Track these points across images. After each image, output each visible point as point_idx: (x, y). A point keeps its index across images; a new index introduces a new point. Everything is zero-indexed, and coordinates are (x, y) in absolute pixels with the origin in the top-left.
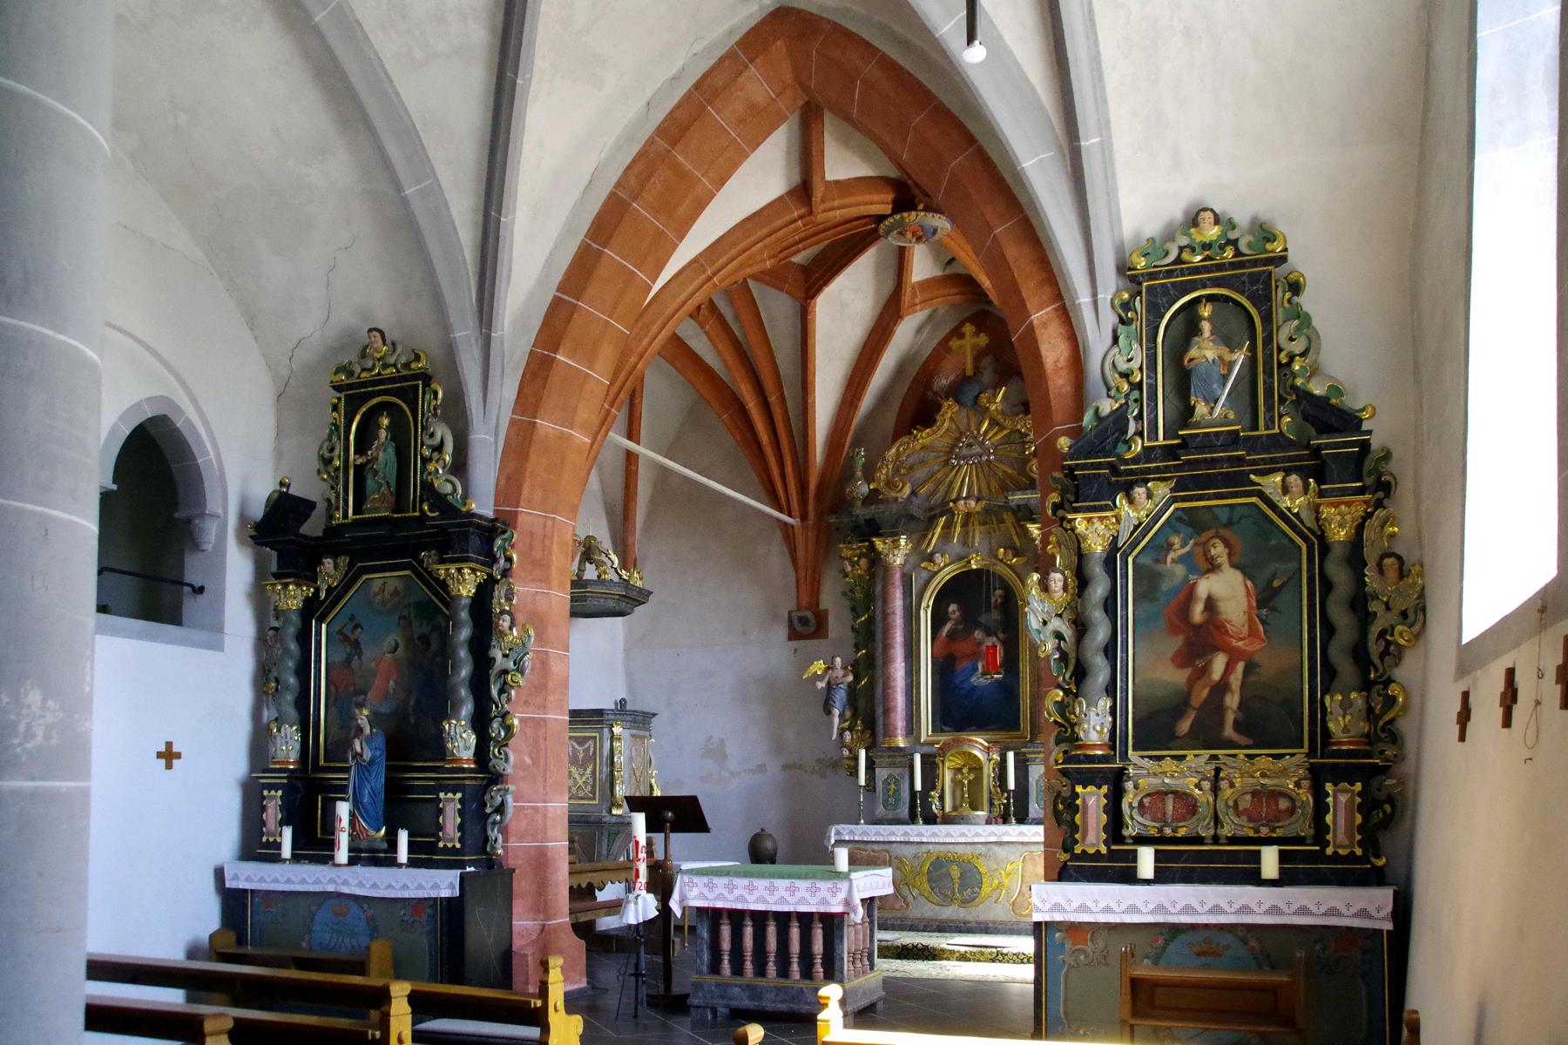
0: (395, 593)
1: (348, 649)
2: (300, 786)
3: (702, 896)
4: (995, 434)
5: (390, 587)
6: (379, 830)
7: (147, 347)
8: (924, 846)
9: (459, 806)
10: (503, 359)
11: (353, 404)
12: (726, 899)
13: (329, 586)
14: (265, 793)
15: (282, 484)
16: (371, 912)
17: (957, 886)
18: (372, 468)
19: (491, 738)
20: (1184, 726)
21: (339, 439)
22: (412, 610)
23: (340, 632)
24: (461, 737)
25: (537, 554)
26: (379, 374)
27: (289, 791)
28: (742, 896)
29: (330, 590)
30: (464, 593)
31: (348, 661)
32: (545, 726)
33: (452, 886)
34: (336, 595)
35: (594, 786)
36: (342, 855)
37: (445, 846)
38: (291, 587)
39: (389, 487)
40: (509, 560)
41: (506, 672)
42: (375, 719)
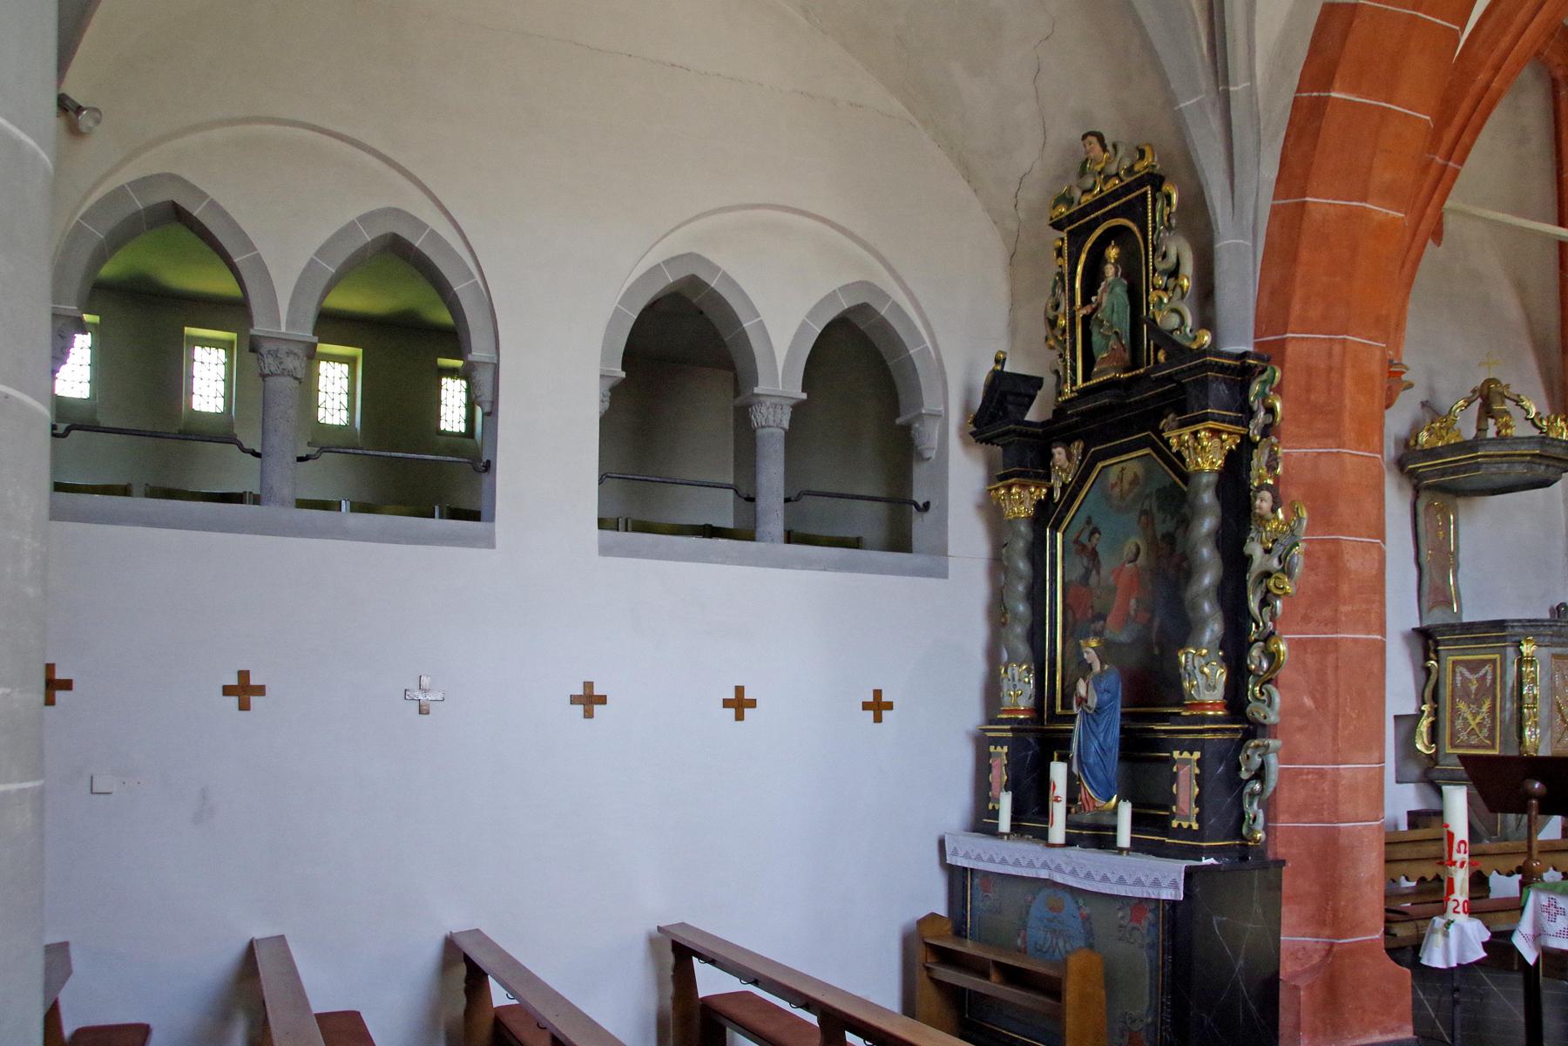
0: (1135, 481)
2: (1031, 740)
5: (1129, 476)
6: (1109, 799)
7: (834, 225)
9: (1197, 771)
10: (1259, 124)
11: (1076, 239)
13: (1063, 483)
14: (992, 749)
15: (997, 361)
16: (1086, 911)
18: (1097, 318)
19: (1250, 672)
21: (1064, 290)
23: (1076, 542)
24: (1202, 672)
25: (1318, 397)
26: (1101, 191)
27: (1016, 746)
29: (1064, 487)
30: (1207, 467)
31: (1086, 577)
32: (1336, 650)
33: (1174, 885)
34: (1071, 493)
35: (1492, 729)
36: (1058, 832)
37: (1180, 825)
38: (1014, 491)
39: (1120, 340)
40: (1270, 410)
41: (1267, 575)
42: (1105, 652)
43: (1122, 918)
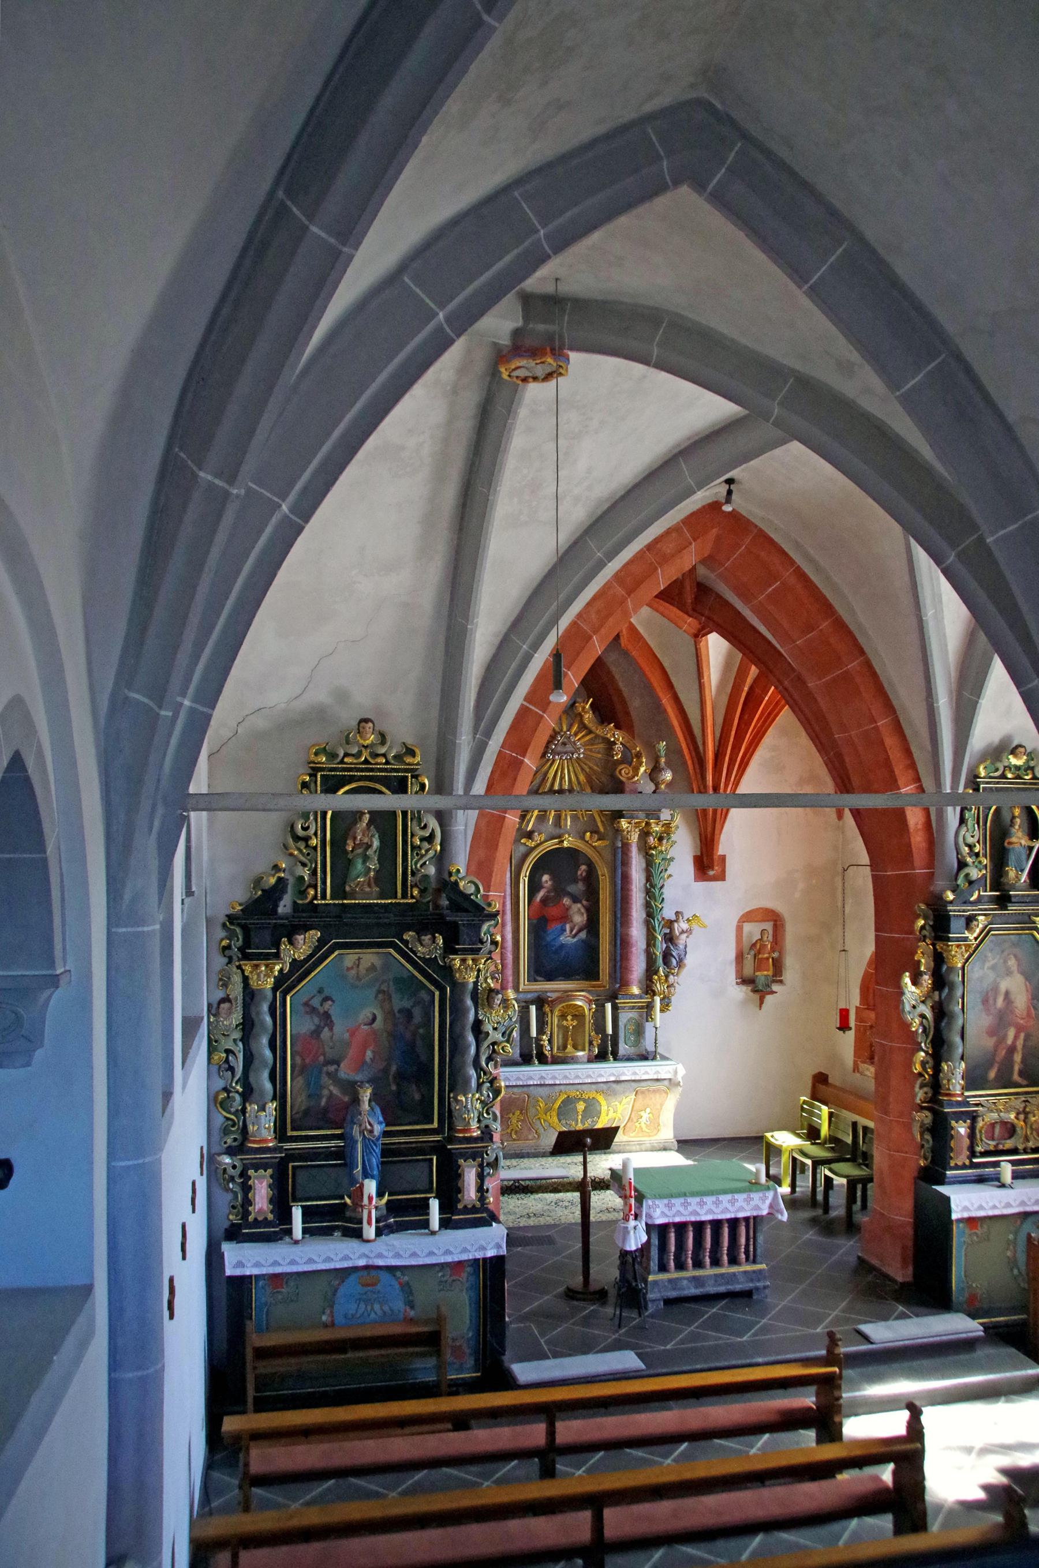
1: (316, 1020)
3: (663, 1214)
4: (583, 737)
8: (557, 1087)
12: (682, 1214)
16: (406, 1278)
17: (580, 1117)
20: (992, 1074)
22: (391, 983)
28: (695, 1210)
31: (316, 1033)
43: (443, 1276)
